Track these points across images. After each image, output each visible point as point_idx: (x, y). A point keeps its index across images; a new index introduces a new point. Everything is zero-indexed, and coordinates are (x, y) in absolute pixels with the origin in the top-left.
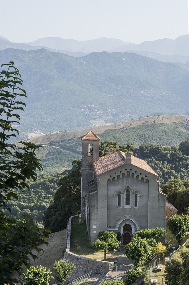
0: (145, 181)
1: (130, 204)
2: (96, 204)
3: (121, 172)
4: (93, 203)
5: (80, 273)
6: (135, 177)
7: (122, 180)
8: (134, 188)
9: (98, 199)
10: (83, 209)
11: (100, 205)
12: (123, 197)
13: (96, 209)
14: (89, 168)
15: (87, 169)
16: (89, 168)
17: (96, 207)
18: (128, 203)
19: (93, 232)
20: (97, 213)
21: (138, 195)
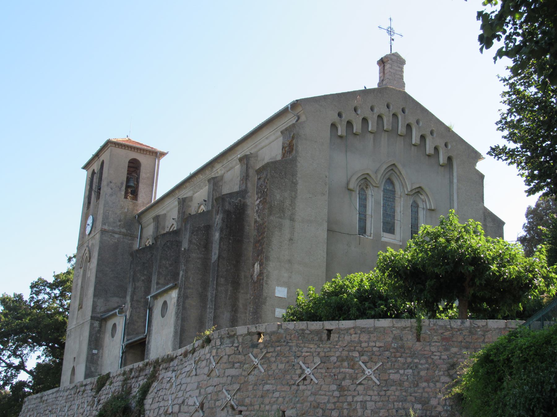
0: (442, 159)
1: (397, 229)
2: (287, 203)
3: (372, 109)
4: (278, 197)
5: (359, 398)
6: (415, 139)
7: (374, 139)
8: (410, 177)
9: (295, 184)
10: (93, 354)
11: (303, 209)
12: (375, 198)
13: (287, 223)
14: (123, 230)
15: (116, 230)
16: (123, 230)
17: (289, 213)
18: (389, 228)
19: (274, 312)
20: (291, 239)
21: (421, 205)
